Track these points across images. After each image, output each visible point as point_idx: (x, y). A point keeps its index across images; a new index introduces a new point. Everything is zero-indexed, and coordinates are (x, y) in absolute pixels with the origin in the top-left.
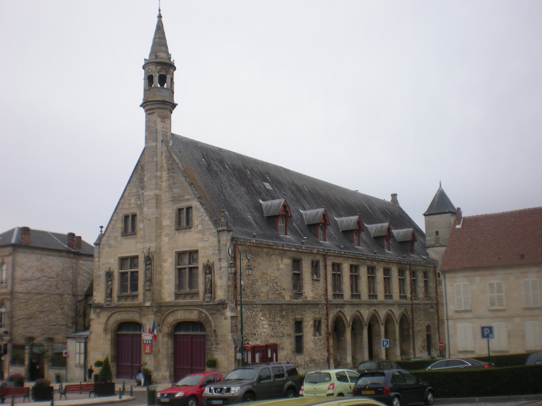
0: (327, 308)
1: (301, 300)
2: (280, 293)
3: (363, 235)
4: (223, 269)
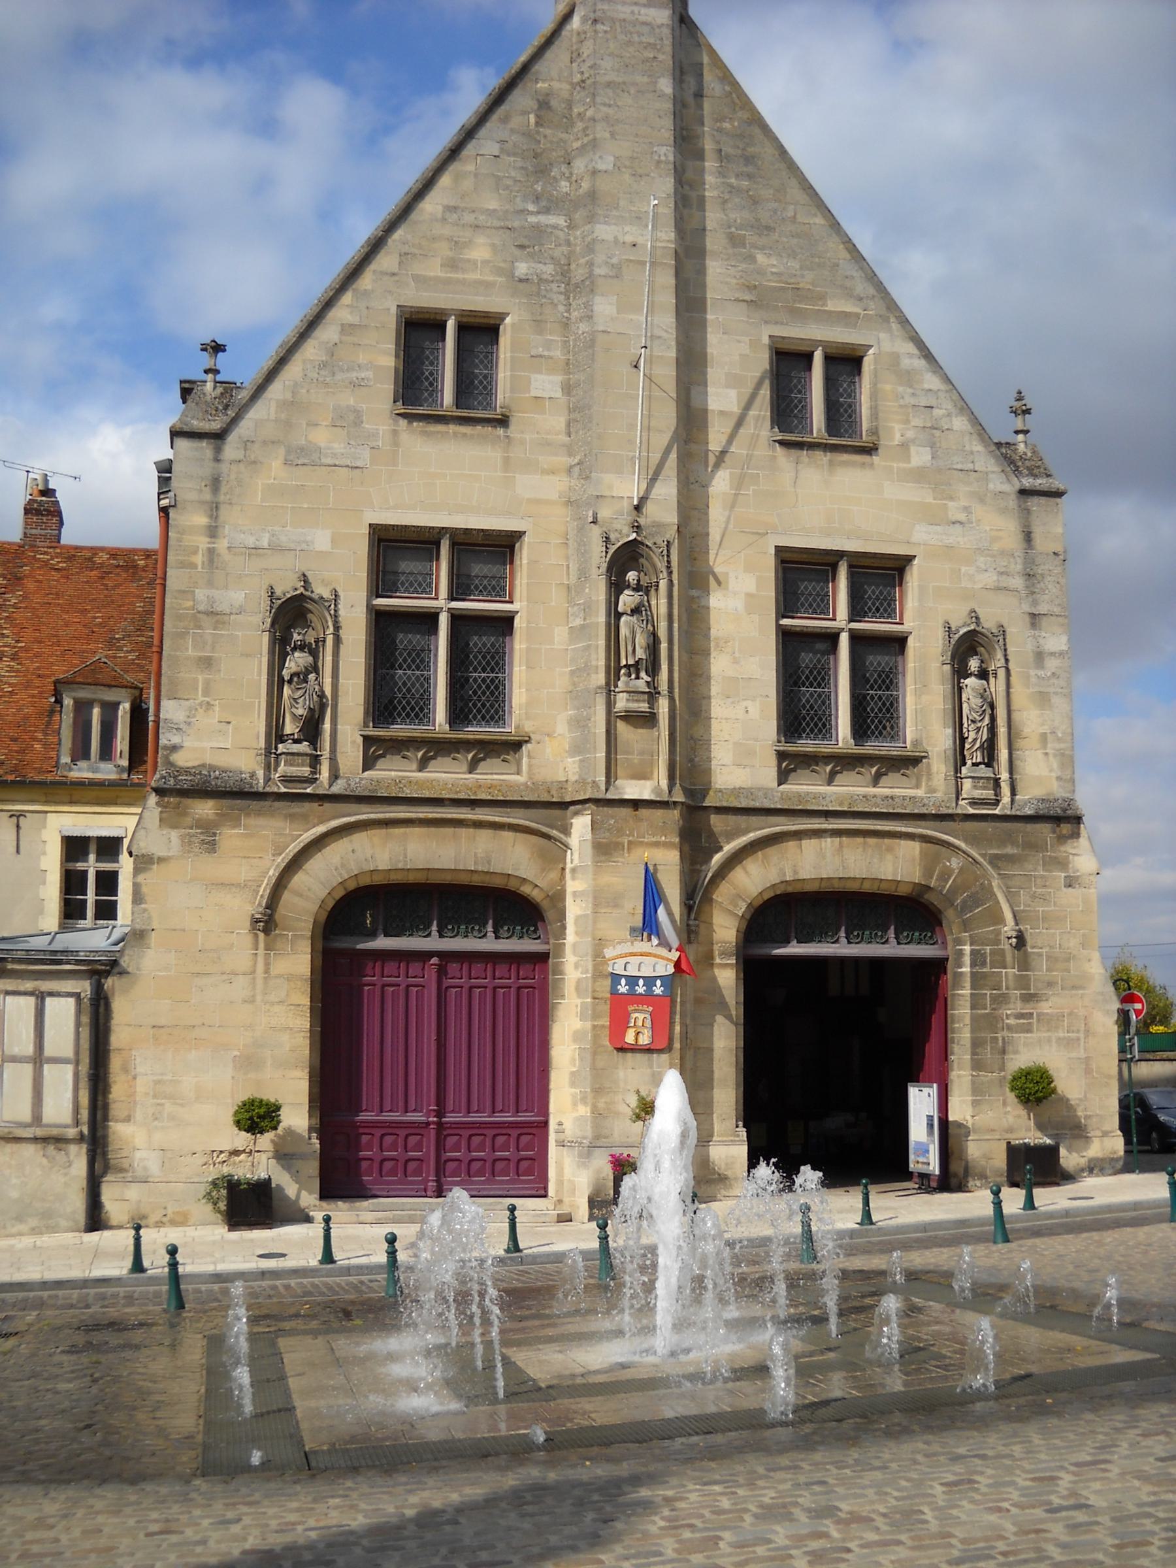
4: (1052, 664)
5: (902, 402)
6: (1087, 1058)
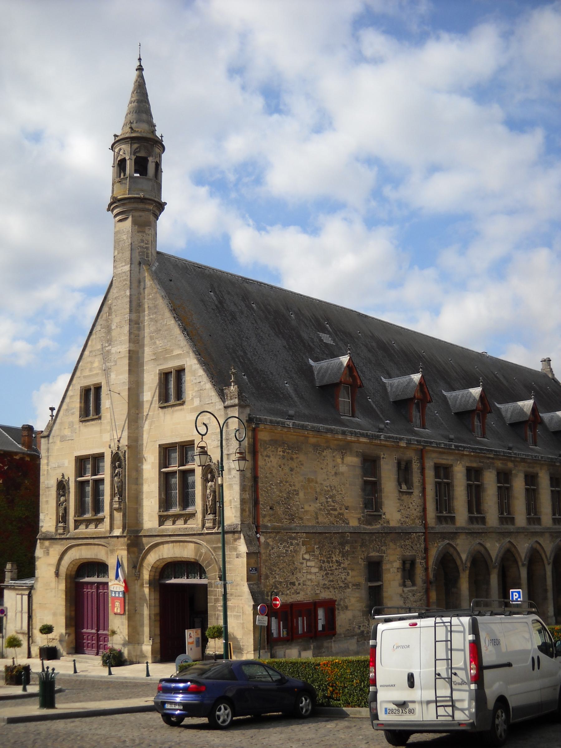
0: (425, 540)
1: (378, 526)
2: (340, 514)
3: (491, 420)
5: (192, 383)
6: (243, 623)
